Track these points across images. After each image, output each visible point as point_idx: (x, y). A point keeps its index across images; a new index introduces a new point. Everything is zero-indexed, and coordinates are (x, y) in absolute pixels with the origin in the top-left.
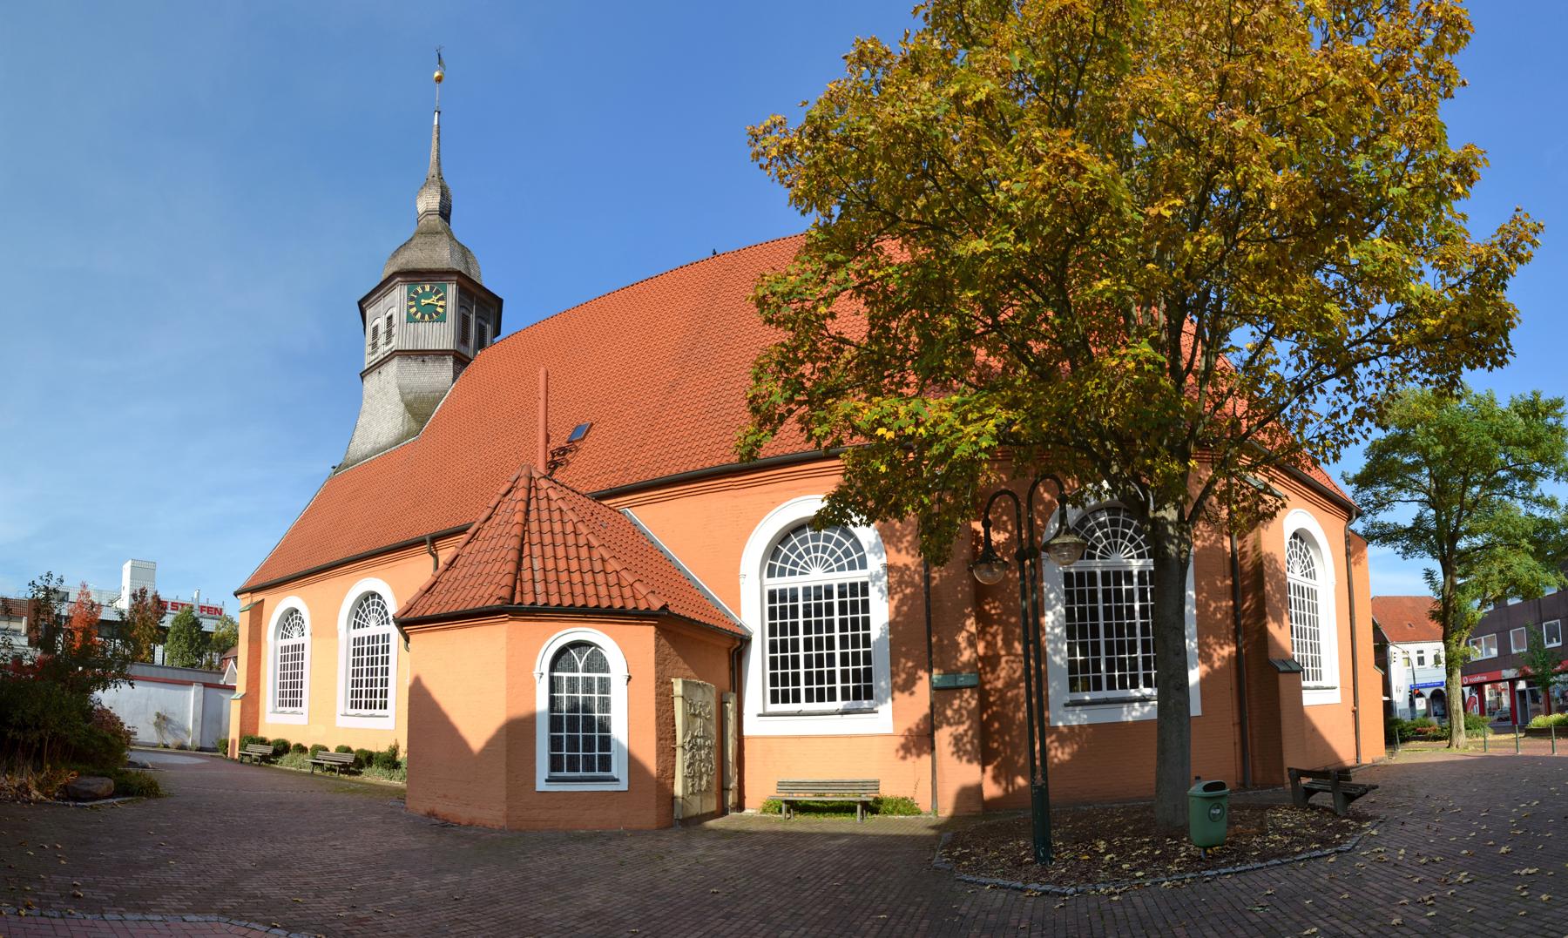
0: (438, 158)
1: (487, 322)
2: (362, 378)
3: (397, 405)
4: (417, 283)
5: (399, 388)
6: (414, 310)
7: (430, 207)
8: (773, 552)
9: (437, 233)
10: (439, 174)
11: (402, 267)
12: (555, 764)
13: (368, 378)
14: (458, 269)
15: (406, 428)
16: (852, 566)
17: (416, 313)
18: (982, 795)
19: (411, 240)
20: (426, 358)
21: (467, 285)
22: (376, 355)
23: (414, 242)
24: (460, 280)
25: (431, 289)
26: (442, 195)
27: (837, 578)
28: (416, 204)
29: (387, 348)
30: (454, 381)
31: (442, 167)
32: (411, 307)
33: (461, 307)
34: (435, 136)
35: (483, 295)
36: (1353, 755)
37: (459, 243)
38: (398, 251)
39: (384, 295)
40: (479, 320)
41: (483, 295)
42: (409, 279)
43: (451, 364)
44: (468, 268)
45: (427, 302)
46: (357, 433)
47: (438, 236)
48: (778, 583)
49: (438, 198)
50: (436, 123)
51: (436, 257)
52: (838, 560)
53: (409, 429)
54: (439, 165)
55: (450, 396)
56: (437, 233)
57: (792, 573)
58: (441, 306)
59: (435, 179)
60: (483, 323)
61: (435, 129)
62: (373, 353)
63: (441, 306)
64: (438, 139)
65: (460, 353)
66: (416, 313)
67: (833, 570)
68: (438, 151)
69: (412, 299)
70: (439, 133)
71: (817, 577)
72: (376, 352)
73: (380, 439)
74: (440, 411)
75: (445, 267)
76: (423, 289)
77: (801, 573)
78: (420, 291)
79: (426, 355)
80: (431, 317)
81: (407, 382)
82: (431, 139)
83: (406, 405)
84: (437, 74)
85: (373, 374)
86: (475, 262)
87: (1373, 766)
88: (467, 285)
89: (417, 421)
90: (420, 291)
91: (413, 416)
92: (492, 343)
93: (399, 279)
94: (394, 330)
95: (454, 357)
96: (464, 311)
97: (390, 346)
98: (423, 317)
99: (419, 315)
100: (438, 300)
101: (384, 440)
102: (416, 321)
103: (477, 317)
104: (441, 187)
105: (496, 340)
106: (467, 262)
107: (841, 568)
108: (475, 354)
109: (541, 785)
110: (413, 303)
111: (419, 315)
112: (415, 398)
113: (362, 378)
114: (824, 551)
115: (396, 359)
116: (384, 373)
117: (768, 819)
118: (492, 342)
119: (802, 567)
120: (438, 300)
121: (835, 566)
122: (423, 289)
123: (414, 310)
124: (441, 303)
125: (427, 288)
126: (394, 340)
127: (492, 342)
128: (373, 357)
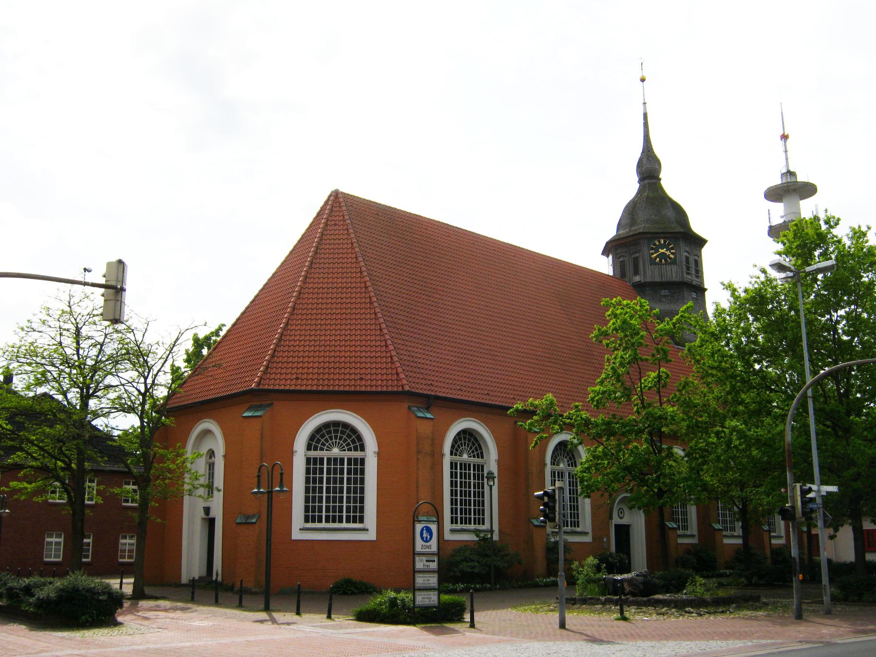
8: (312, 438)
12: (454, 521)
16: (356, 449)
27: (347, 454)
48: (313, 454)
52: (348, 445)
57: (322, 449)
67: (345, 450)
71: (336, 451)
76: (659, 242)
77: (326, 450)
78: (658, 243)
87: (869, 561)
90: (658, 243)
102: (655, 264)
107: (350, 450)
109: (296, 535)
114: (327, 441)
117: (20, 575)
119: (342, 444)
121: (346, 448)
122: (659, 242)
125: (662, 241)
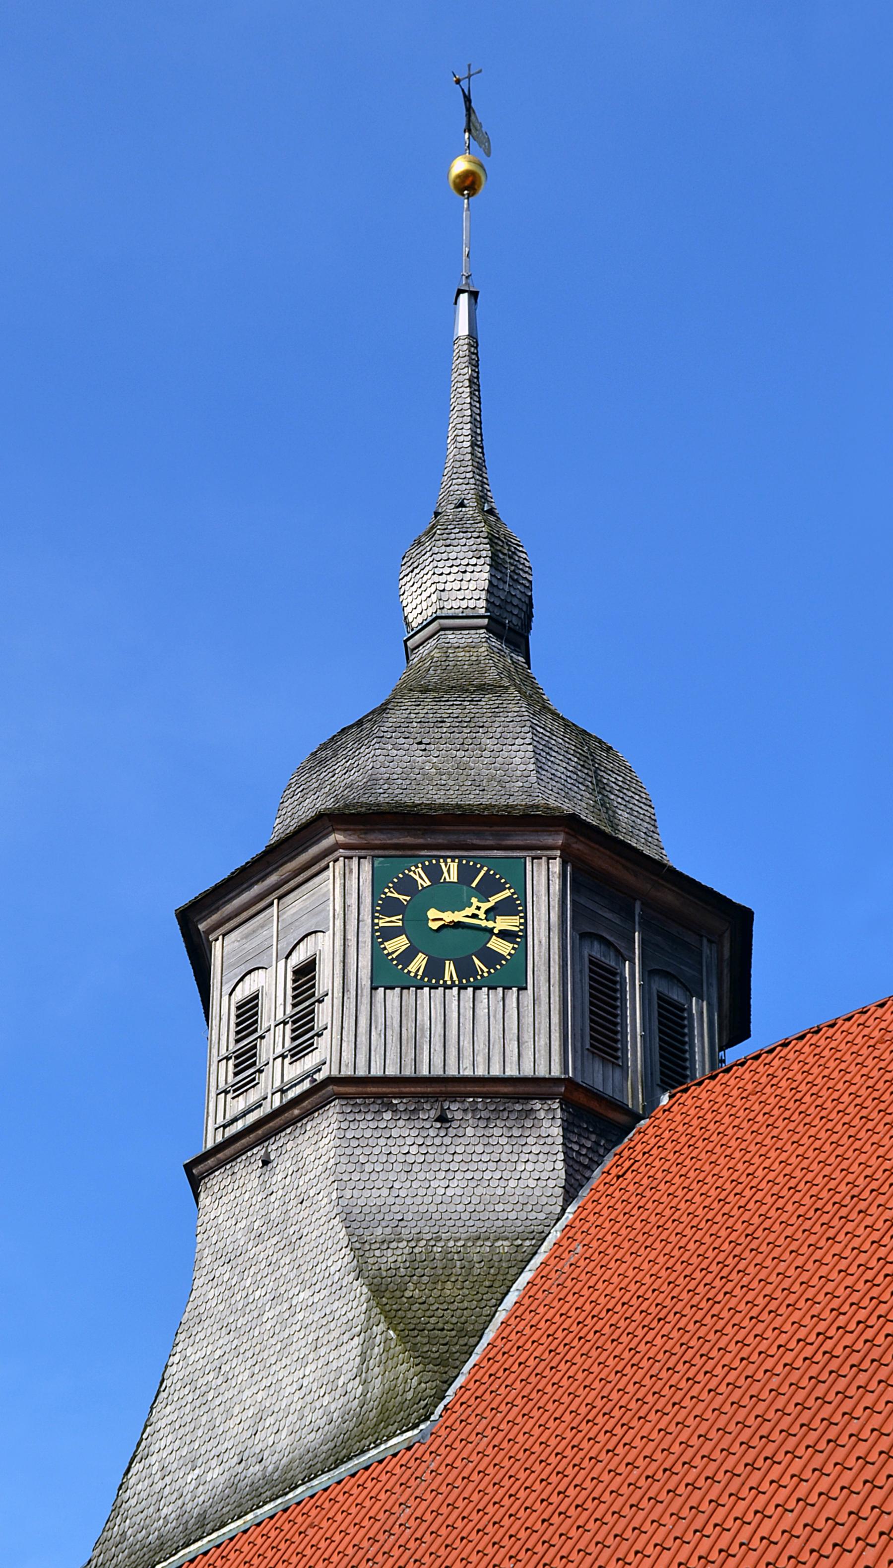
0: (476, 444)
1: (693, 989)
2: (195, 1183)
3: (338, 1291)
4: (409, 851)
5: (348, 1220)
6: (398, 944)
7: (453, 604)
9: (482, 688)
10: (482, 497)
11: (352, 796)
13: (218, 1181)
14: (567, 807)
15: (377, 1387)
17: (407, 957)
18: (488, 942)
19: (383, 709)
20: (454, 1109)
21: (602, 861)
22: (253, 1096)
23: (395, 717)
24: (578, 846)
25: (465, 875)
26: (496, 564)
28: (398, 594)
29: (293, 1071)
30: (570, 1193)
31: (490, 474)
32: (389, 934)
33: (584, 936)
34: (462, 373)
35: (669, 897)
36: (362, 866)
37: (567, 725)
38: (333, 743)
39: (282, 891)
40: (659, 985)
41: (669, 897)
42: (376, 838)
43: (556, 1131)
44: (604, 805)
45: (449, 917)
46: (164, 1415)
47: (487, 701)
49: (482, 576)
50: (462, 328)
51: (479, 766)
53: (390, 1392)
54: (480, 467)
55: (557, 1254)
56: (482, 688)
58: (504, 935)
59: (470, 511)
60: (676, 995)
61: (462, 348)
62: (239, 1089)
63: (504, 935)
64: (474, 383)
65: (591, 1093)
66: (407, 957)
68: (476, 422)
69: (389, 907)
70: (474, 363)
72: (251, 1083)
73: (266, 1438)
74: (516, 1315)
75: (519, 800)
76: (434, 873)
78: (424, 881)
79: (453, 1097)
80: (465, 970)
81: (377, 1197)
82: (446, 409)
83: (378, 1290)
84: (460, 165)
85: (238, 1166)
86: (632, 783)
88: (602, 861)
89: (422, 1358)
90: (424, 881)
91: (403, 1338)
92: (717, 1067)
93: (339, 837)
94: (324, 1014)
95: (566, 1104)
96: (596, 950)
97: (309, 1062)
98: (434, 970)
99: (419, 963)
100: (491, 913)
101: (284, 1440)
103: (648, 973)
104: (492, 540)
105: (733, 1054)
106: (600, 787)
108: (651, 1103)
110: (396, 921)
111: (419, 963)
112: (413, 1262)
113: (195, 1183)
115: (333, 1113)
116: (283, 1165)
118: (716, 1061)
120: (491, 913)
122: (434, 873)
123: (398, 944)
124: (502, 923)
125: (451, 872)
126: (323, 1049)
127: (716, 1061)
128: (241, 1104)
